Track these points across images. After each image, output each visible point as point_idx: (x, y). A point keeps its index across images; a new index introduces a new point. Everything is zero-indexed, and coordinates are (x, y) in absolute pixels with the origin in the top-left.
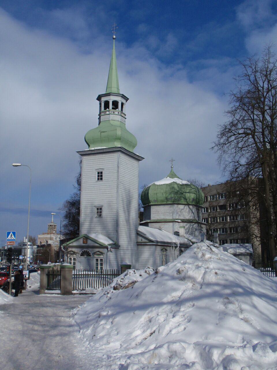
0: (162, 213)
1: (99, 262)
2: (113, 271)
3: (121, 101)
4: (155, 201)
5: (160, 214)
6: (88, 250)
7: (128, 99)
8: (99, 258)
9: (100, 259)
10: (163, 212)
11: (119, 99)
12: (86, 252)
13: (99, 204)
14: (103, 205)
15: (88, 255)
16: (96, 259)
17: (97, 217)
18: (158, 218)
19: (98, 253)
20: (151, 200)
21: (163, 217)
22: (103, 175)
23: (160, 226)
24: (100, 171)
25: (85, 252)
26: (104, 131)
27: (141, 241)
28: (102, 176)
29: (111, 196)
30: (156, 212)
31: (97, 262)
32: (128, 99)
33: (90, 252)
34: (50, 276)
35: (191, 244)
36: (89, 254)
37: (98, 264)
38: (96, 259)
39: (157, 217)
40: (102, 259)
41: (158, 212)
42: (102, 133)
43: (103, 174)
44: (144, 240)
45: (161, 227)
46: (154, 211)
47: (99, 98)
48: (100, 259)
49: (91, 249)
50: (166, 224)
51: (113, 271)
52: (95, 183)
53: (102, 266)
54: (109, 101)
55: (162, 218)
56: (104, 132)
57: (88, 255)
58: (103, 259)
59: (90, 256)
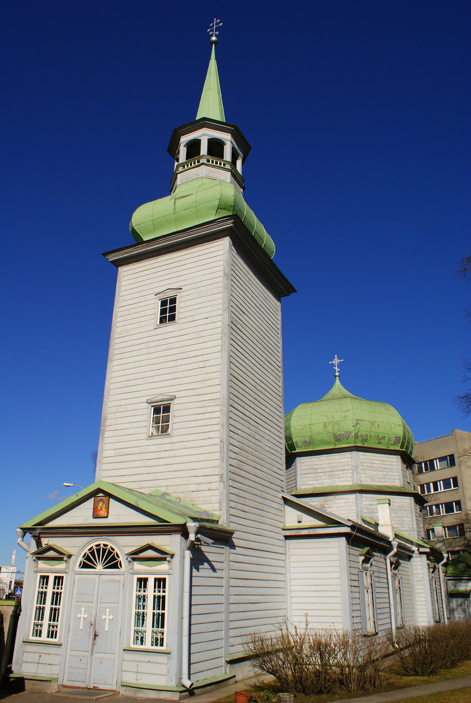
0: (326, 472)
1: (150, 592)
2: (280, 577)
3: (231, 142)
4: (306, 443)
5: (321, 474)
6: (110, 545)
9: (156, 579)
10: (327, 470)
16: (140, 580)
17: (155, 433)
18: (316, 486)
19: (150, 553)
20: (297, 443)
21: (328, 481)
22: (178, 305)
23: (322, 503)
25: (98, 551)
26: (183, 195)
27: (297, 525)
28: (173, 309)
29: (202, 365)
30: (310, 471)
33: (117, 550)
35: (446, 528)
36: (113, 559)
37: (144, 598)
40: (164, 580)
41: (316, 469)
43: (176, 313)
44: (308, 521)
45: (326, 506)
46: (303, 468)
48: (156, 579)
50: (339, 499)
51: (280, 577)
53: (163, 609)
54: (200, 138)
55: (326, 485)
58: (167, 577)
59: (115, 566)
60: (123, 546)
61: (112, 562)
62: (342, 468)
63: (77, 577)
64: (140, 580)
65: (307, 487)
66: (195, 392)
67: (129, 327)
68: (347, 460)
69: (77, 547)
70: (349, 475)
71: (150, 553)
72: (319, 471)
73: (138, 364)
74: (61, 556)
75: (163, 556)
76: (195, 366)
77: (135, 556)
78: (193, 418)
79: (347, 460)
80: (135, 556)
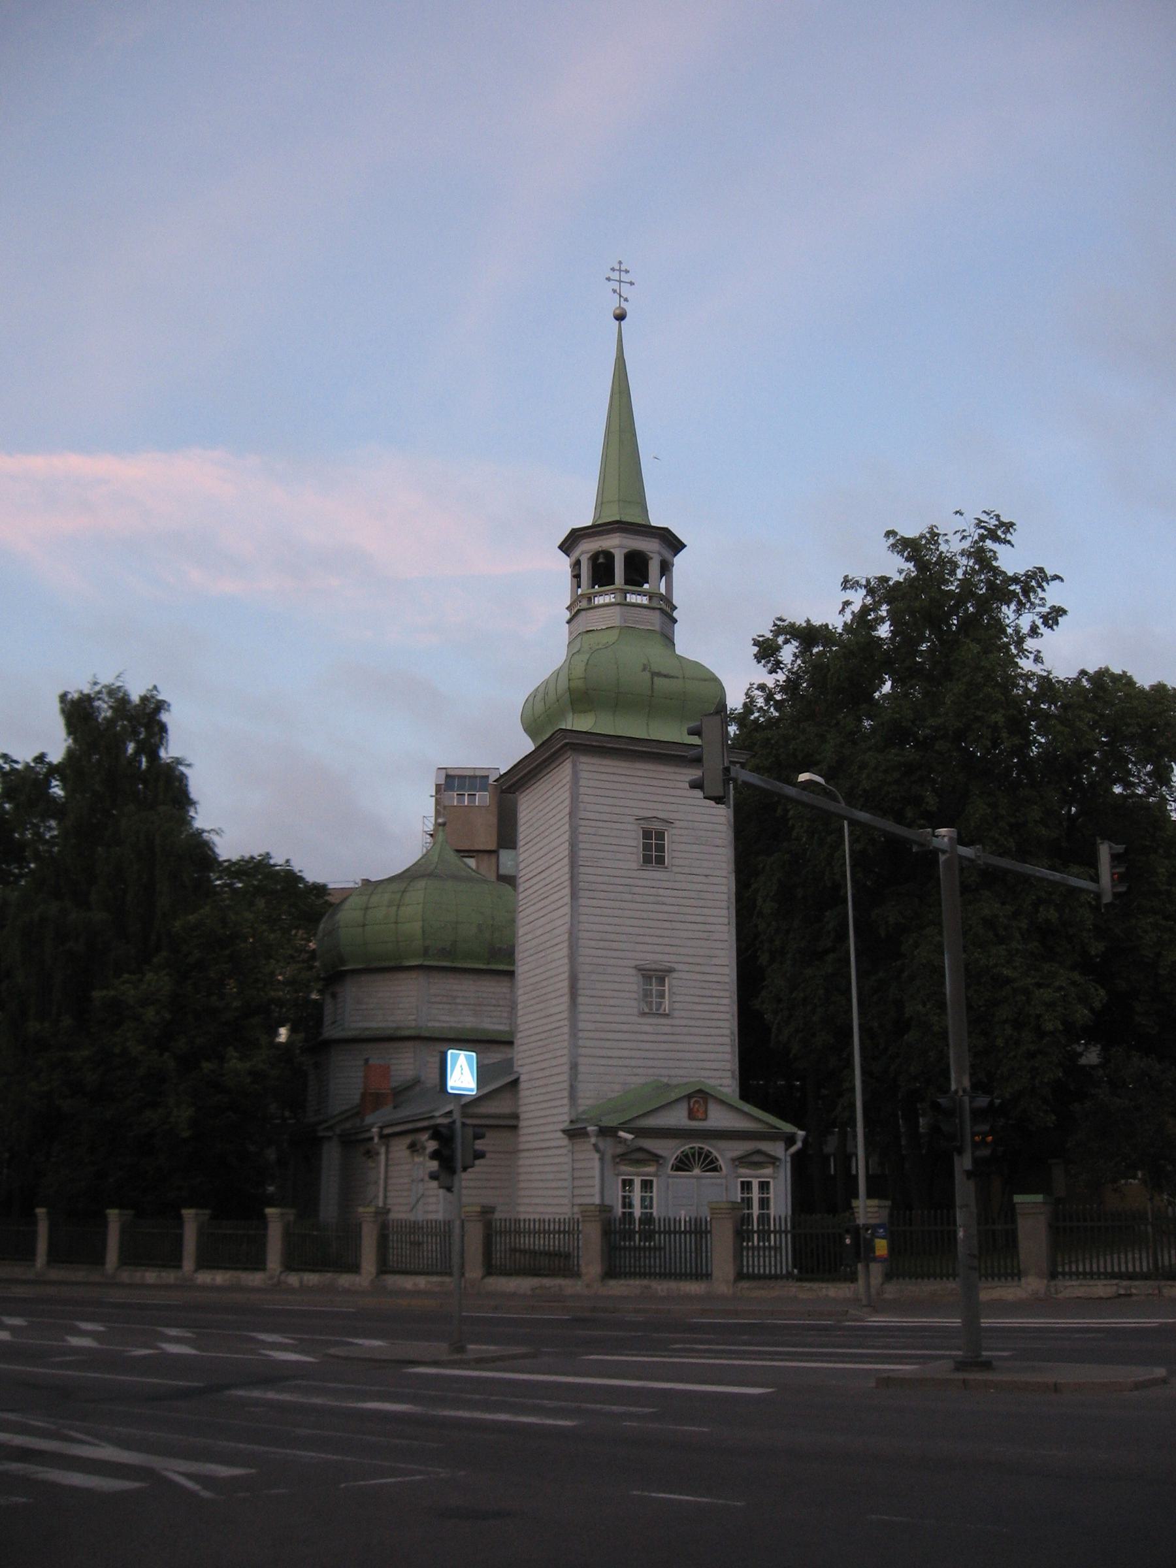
1: (755, 1194)
3: (660, 553)
5: (461, 1007)
6: (707, 1148)
7: (684, 546)
8: (638, 1175)
11: (649, 546)
12: (707, 1156)
13: (655, 962)
14: (675, 966)
15: (709, 1164)
16: (624, 1181)
18: (454, 1025)
24: (657, 826)
29: (705, 935)
31: (746, 1195)
32: (684, 546)
34: (772, 1236)
38: (742, 1183)
39: (443, 1018)
41: (456, 997)
42: (655, 678)
47: (567, 546)
49: (723, 1144)
52: (635, 874)
54: (651, 555)
55: (468, 1025)
56: (665, 676)
57: (709, 1164)
59: (715, 1169)
60: (725, 1152)
61: (711, 1165)
62: (494, 1002)
63: (670, 1180)
64: (624, 1181)
65: (437, 1024)
66: (698, 968)
67: (601, 855)
68: (504, 990)
69: (670, 1150)
70: (505, 1015)
71: (756, 1158)
72: (458, 1001)
73: (617, 912)
74: (656, 1158)
75: (773, 1161)
76: (697, 935)
77: (742, 1161)
78: (697, 1000)
79: (504, 990)
80: (742, 1161)
